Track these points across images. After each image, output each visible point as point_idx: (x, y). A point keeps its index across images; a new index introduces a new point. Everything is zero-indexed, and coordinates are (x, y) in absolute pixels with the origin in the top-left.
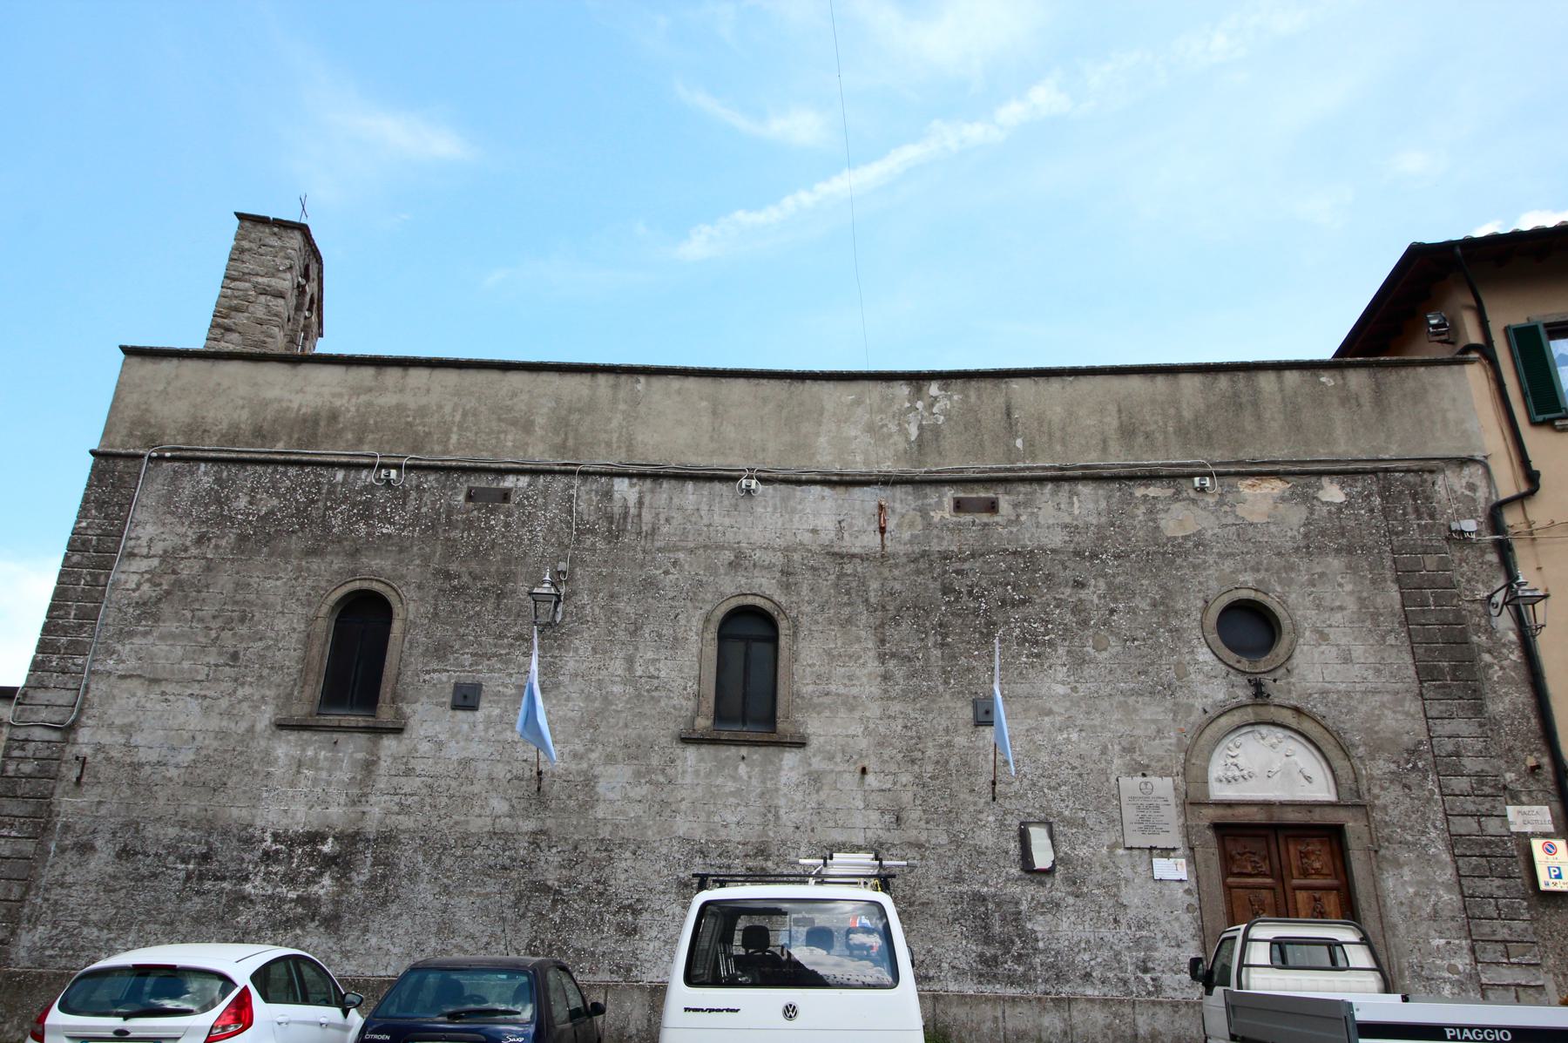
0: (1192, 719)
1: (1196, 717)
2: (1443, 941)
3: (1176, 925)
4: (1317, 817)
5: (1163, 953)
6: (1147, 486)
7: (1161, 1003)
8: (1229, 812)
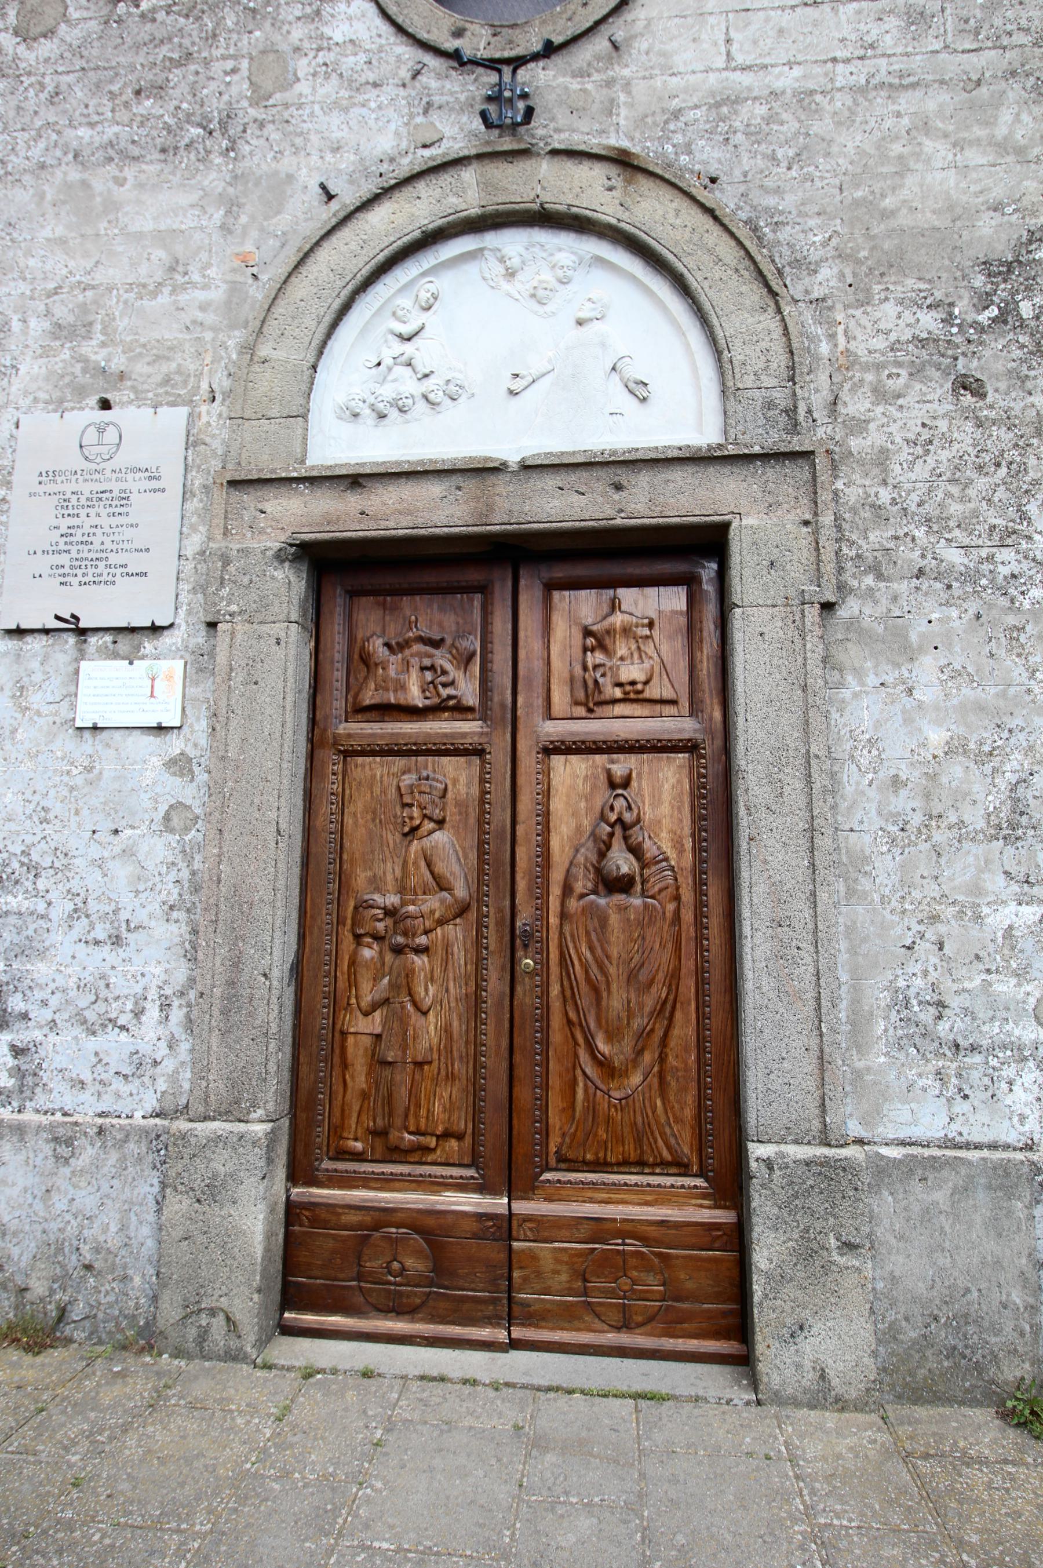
0: (282, 222)
1: (304, 214)
3: (122, 872)
4: (644, 503)
7: (20, 1130)
8: (353, 501)
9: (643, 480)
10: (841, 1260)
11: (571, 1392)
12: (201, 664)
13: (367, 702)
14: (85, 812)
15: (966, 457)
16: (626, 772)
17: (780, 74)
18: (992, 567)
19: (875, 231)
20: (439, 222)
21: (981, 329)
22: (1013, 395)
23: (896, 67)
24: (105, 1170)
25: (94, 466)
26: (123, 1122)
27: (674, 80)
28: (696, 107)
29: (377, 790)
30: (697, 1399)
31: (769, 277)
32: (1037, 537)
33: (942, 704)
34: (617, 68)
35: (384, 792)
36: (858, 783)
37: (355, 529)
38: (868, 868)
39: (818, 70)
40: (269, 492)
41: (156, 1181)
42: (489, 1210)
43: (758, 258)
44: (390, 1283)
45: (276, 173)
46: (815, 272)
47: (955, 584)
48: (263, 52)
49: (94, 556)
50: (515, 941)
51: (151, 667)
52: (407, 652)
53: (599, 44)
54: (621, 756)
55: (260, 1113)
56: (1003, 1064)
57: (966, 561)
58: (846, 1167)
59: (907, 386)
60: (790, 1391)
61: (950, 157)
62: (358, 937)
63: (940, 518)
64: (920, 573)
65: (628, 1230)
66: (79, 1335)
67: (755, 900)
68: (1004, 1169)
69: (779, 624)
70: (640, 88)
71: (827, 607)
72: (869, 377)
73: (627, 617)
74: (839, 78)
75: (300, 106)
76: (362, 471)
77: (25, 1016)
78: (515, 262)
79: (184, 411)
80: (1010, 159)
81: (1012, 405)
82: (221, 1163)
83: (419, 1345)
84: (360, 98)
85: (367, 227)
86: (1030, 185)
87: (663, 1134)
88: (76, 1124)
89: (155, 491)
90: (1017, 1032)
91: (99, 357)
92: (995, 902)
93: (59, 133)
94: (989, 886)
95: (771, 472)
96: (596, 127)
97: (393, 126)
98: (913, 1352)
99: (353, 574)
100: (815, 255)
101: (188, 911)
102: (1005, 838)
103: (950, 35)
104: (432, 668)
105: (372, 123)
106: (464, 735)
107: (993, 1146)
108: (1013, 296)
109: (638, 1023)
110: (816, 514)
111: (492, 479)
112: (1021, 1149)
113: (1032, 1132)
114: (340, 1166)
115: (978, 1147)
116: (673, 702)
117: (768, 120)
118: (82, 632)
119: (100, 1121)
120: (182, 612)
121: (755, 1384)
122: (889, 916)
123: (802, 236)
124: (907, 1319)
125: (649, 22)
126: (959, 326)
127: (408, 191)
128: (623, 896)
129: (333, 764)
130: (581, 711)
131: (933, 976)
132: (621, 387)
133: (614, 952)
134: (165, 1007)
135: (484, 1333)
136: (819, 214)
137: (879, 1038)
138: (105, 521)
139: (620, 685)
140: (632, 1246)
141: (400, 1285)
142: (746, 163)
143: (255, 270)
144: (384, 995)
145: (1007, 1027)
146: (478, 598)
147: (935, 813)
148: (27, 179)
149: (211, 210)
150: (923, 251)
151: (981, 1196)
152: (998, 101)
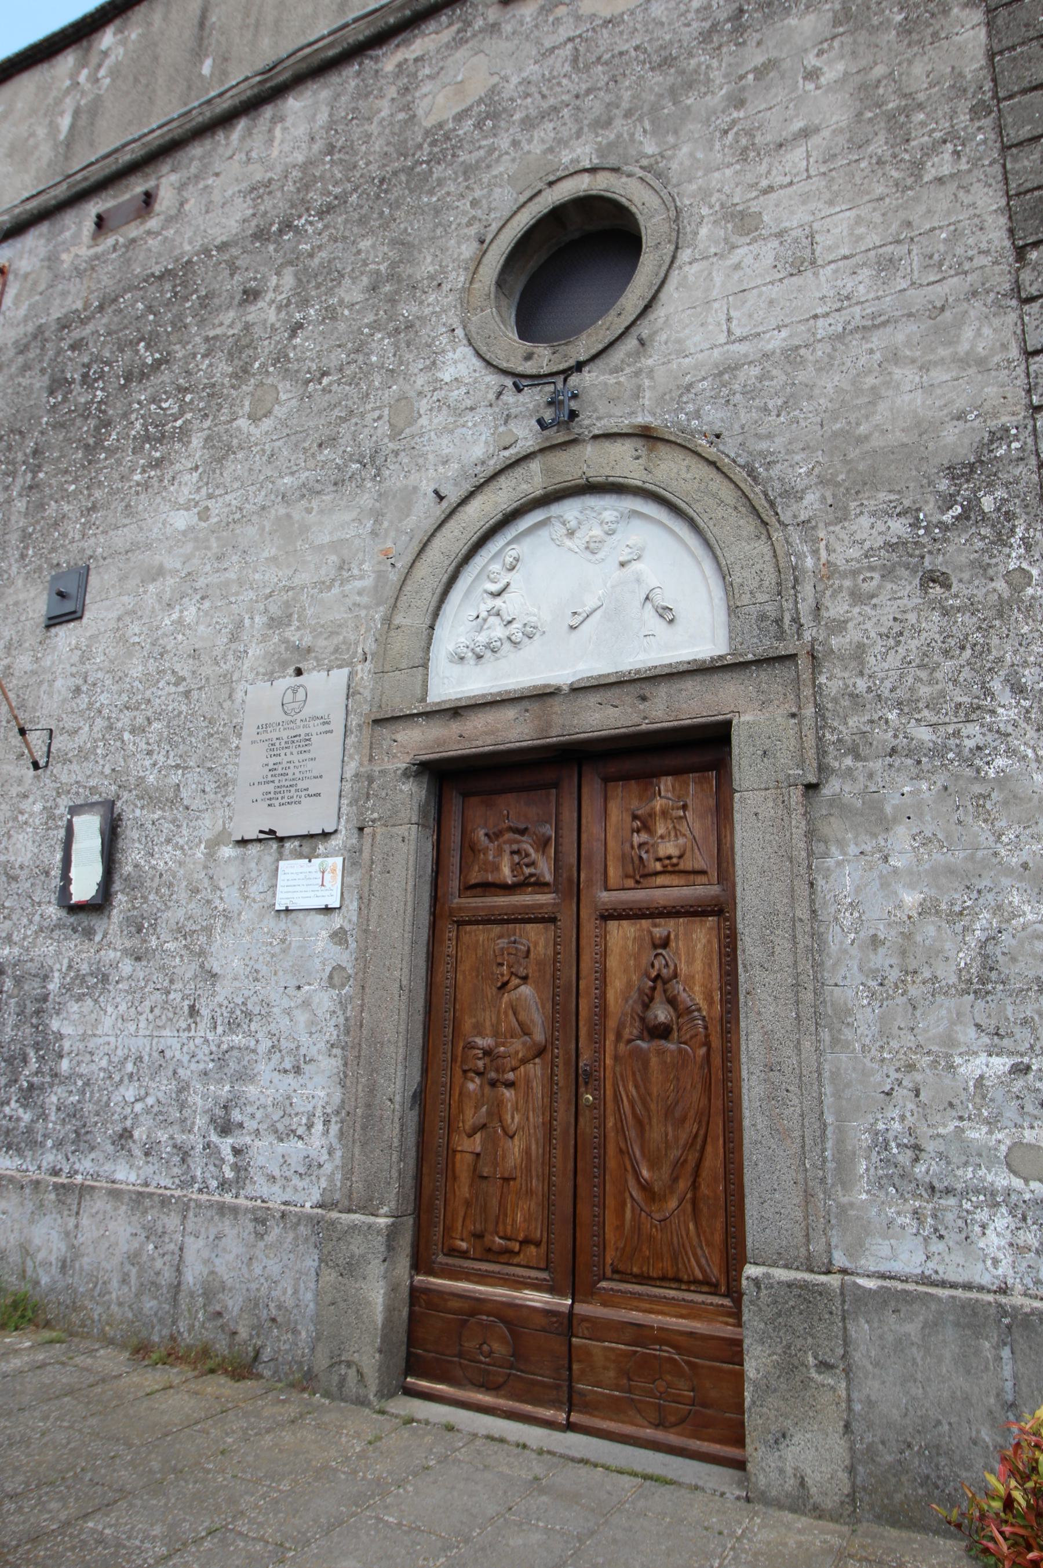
1: (424, 512)
2: (1001, 1064)
3: (302, 1017)
4: (662, 712)
5: (267, 1086)
6: (407, 43)
7: (235, 1210)
8: (455, 728)
9: (662, 692)
10: (819, 1378)
11: (596, 1466)
12: (353, 860)
13: (473, 881)
14: (280, 973)
15: (933, 644)
16: (666, 933)
17: (771, 338)
18: (958, 741)
19: (851, 456)
20: (515, 505)
21: (945, 527)
22: (976, 583)
23: (869, 311)
24: (285, 1246)
25: (289, 718)
26: (297, 1209)
27: (687, 360)
28: (704, 379)
29: (480, 953)
30: (697, 1488)
31: (761, 510)
32: (1000, 710)
33: (915, 869)
34: (643, 360)
35: (485, 953)
36: (841, 943)
37: (456, 749)
38: (850, 1020)
39: (802, 328)
40: (400, 726)
41: (316, 1257)
42: (554, 1308)
43: (752, 496)
44: (481, 1362)
45: (406, 486)
46: (802, 498)
47: (924, 760)
48: (398, 400)
49: (288, 783)
50: (581, 1079)
51: (322, 864)
52: (501, 840)
53: (631, 343)
54: (662, 921)
55: (385, 1210)
56: (976, 1207)
57: (934, 738)
58: (822, 1291)
59: (879, 587)
60: (774, 1493)
61: (917, 379)
62: (465, 1072)
63: (910, 701)
64: (893, 751)
65: (663, 1337)
66: (267, 1373)
67: (751, 1047)
68: (971, 1309)
69: (771, 804)
70: (660, 373)
71: (811, 788)
72: (847, 583)
73: (664, 801)
74: (820, 331)
75: (422, 435)
76: (459, 704)
77: (241, 1125)
78: (573, 524)
79: (346, 671)
80: (972, 371)
81: (975, 592)
82: (356, 1246)
83: (499, 1416)
84: (461, 421)
85: (465, 517)
86: (991, 391)
87: (695, 1255)
88: (268, 1209)
89: (326, 732)
90: (989, 1178)
91: (295, 638)
92: (967, 1053)
93: (273, 483)
94: (961, 1038)
95: (763, 675)
96: (628, 410)
97: (483, 438)
98: (890, 1476)
99: (458, 782)
100: (800, 485)
101: (343, 1048)
102: (975, 992)
103: (916, 273)
104: (517, 852)
105: (469, 438)
106: (541, 906)
107: (968, 1287)
108: (975, 493)
109: (675, 1153)
110: (800, 708)
111: (550, 701)
112: (995, 1292)
113: (1005, 1277)
114: (450, 1261)
115: (953, 1286)
116: (703, 872)
117: (761, 379)
118: (281, 840)
119: (283, 1207)
120: (343, 821)
121: (745, 1482)
122: (869, 1064)
123: (790, 470)
124: (883, 1443)
125: (667, 317)
126: (925, 527)
127: (493, 485)
128: (663, 1042)
129: (450, 932)
130: (630, 883)
131: (910, 1120)
132: (653, 613)
133: (654, 1090)
134: (327, 1122)
135: (548, 1413)
136: (803, 449)
137: (861, 1176)
138: (295, 758)
139: (659, 859)
140: (667, 1352)
141: (489, 1364)
142: (744, 417)
143: (392, 561)
144: (483, 1121)
145: (980, 1173)
146: (554, 791)
147: (910, 969)
148: (255, 518)
149: (365, 521)
150: (893, 467)
151: (950, 1333)
152: (960, 321)
